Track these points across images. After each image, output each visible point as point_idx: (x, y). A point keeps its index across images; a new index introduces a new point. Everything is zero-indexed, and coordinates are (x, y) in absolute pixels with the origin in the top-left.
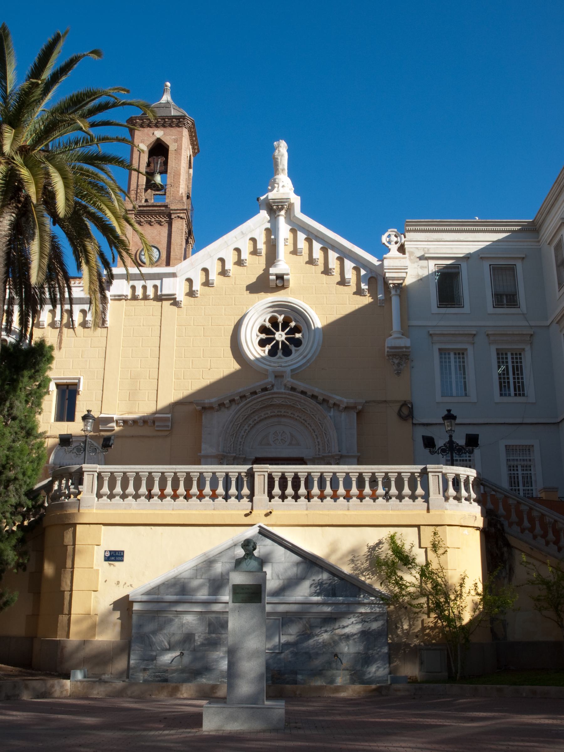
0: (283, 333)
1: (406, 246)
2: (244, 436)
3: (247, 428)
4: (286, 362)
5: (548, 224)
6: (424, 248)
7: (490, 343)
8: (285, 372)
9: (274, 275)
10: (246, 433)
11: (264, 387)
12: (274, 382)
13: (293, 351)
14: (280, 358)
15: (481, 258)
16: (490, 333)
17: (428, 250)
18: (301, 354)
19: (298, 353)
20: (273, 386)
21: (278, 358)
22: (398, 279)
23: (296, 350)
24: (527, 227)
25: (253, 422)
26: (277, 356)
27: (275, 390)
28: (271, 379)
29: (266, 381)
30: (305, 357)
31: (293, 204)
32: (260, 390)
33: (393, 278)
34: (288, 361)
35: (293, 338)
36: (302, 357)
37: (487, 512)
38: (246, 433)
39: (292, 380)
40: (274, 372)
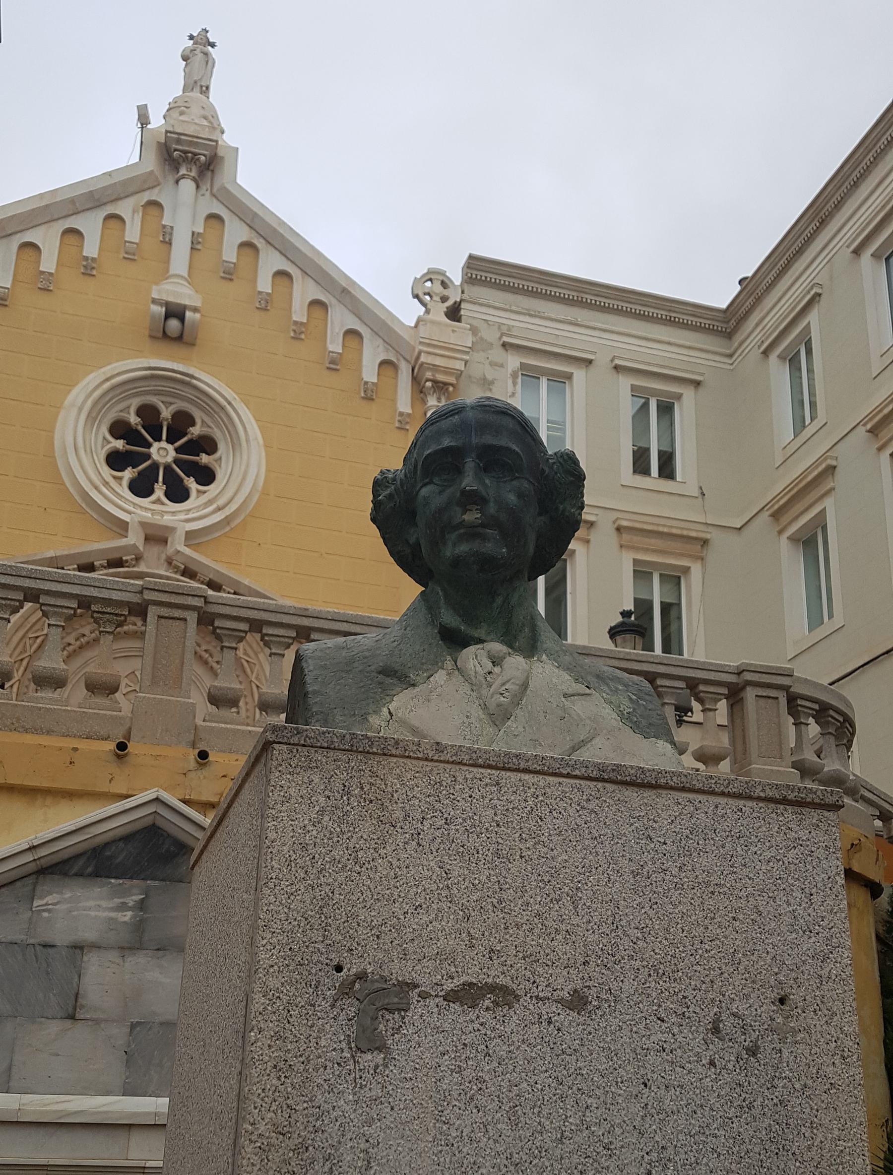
0: (170, 448)
1: (462, 312)
2: (71, 648)
3: (72, 642)
4: (174, 512)
5: (743, 337)
6: (500, 325)
7: (621, 546)
8: (172, 530)
9: (161, 305)
10: (78, 643)
11: (116, 555)
12: (141, 548)
13: (193, 494)
14: (158, 501)
15: (617, 368)
16: (625, 523)
17: (509, 330)
18: (210, 502)
19: (204, 499)
20: (138, 559)
21: (154, 502)
22: (447, 371)
23: (198, 491)
24: (709, 322)
25: (77, 639)
26: (153, 497)
27: (142, 568)
28: (134, 538)
29: (123, 542)
30: (219, 509)
31: (222, 158)
32: (105, 562)
33: (435, 368)
34: (180, 511)
35: (196, 464)
36: (214, 506)
37: (671, 410)
38: (78, 643)
39: (187, 551)
40: (143, 525)
